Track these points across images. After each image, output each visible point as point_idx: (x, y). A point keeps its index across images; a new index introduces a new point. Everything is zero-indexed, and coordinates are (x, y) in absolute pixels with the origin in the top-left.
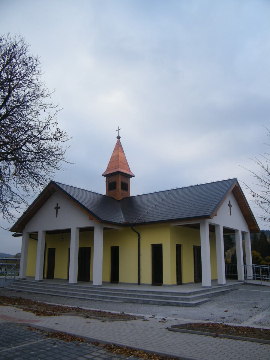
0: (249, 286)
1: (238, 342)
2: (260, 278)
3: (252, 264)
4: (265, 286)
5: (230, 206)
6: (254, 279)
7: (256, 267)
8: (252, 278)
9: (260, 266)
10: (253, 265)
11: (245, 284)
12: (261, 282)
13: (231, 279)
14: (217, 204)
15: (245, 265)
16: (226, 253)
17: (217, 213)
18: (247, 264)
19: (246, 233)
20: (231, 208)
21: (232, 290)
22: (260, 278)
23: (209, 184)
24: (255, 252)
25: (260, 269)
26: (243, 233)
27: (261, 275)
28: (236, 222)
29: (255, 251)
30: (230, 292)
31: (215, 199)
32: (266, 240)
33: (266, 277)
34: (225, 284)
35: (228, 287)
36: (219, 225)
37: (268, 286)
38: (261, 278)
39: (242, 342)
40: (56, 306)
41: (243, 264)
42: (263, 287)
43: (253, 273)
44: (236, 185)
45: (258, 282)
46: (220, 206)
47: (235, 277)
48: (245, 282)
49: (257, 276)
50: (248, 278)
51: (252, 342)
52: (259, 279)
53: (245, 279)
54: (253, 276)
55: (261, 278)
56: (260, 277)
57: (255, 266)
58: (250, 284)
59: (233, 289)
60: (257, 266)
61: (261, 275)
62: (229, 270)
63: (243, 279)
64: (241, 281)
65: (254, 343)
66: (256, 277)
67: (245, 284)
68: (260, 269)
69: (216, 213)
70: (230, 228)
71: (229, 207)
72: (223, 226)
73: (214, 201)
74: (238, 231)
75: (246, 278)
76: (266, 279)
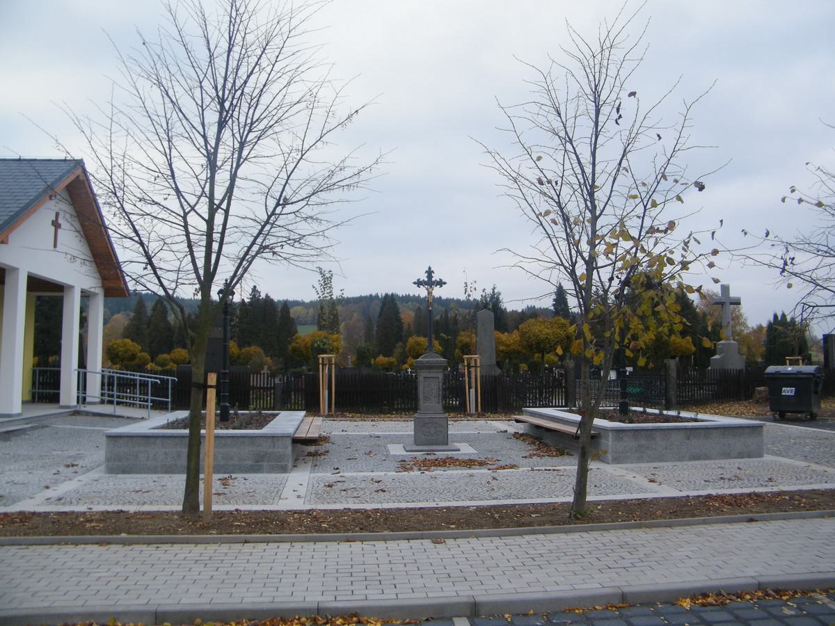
0: (86, 418)
1: (136, 549)
2: (112, 399)
3: (103, 367)
4: (123, 417)
5: (56, 225)
6: (102, 402)
7: (140, 380)
8: (98, 400)
9: (151, 378)
10: (103, 371)
11: (76, 413)
12: (149, 413)
13: (46, 402)
14: (13, 213)
15: (81, 370)
16: (661, 421)
17: (10, 236)
18: (89, 368)
19: (95, 294)
20: (60, 231)
21: (32, 428)
22: (112, 399)
23: (7, 162)
24: (131, 343)
25: (115, 379)
26: (86, 296)
27: (115, 393)
28: (70, 268)
29: (130, 341)
30: (28, 432)
31: (12, 202)
32: (166, 318)
33: (130, 397)
34: (19, 415)
35: (27, 421)
36: (15, 270)
37: (128, 418)
38: (116, 400)
39: (171, 546)
40: (225, 534)
41: (77, 368)
42: (115, 419)
43: (102, 389)
44: (78, 177)
45: (107, 409)
46: (28, 216)
47: (54, 399)
48: (78, 409)
49: (109, 397)
50: (88, 399)
51: (50, 546)
52: (111, 402)
53: (78, 402)
54: (102, 395)
55: (116, 400)
56: (113, 397)
57: (140, 376)
58: (87, 414)
59: (40, 424)
60: (144, 377)
61: (115, 393)
62: (48, 381)
63: (74, 403)
64: (68, 407)
65: (175, 545)
66: (106, 398)
67: (76, 413)
68: (115, 379)
69: (7, 237)
70: (36, 275)
71: (53, 228)
72: (29, 272)
73: (7, 206)
74: (71, 287)
75: (82, 400)
76: (130, 404)
